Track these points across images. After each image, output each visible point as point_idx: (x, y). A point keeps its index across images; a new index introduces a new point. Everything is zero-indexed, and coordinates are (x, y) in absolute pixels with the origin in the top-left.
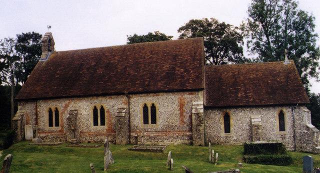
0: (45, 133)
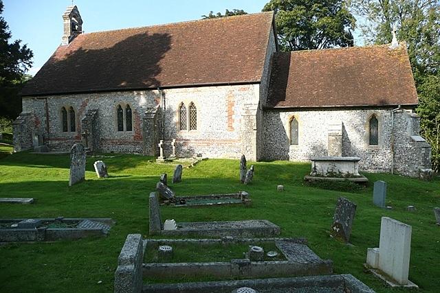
0: (58, 140)
